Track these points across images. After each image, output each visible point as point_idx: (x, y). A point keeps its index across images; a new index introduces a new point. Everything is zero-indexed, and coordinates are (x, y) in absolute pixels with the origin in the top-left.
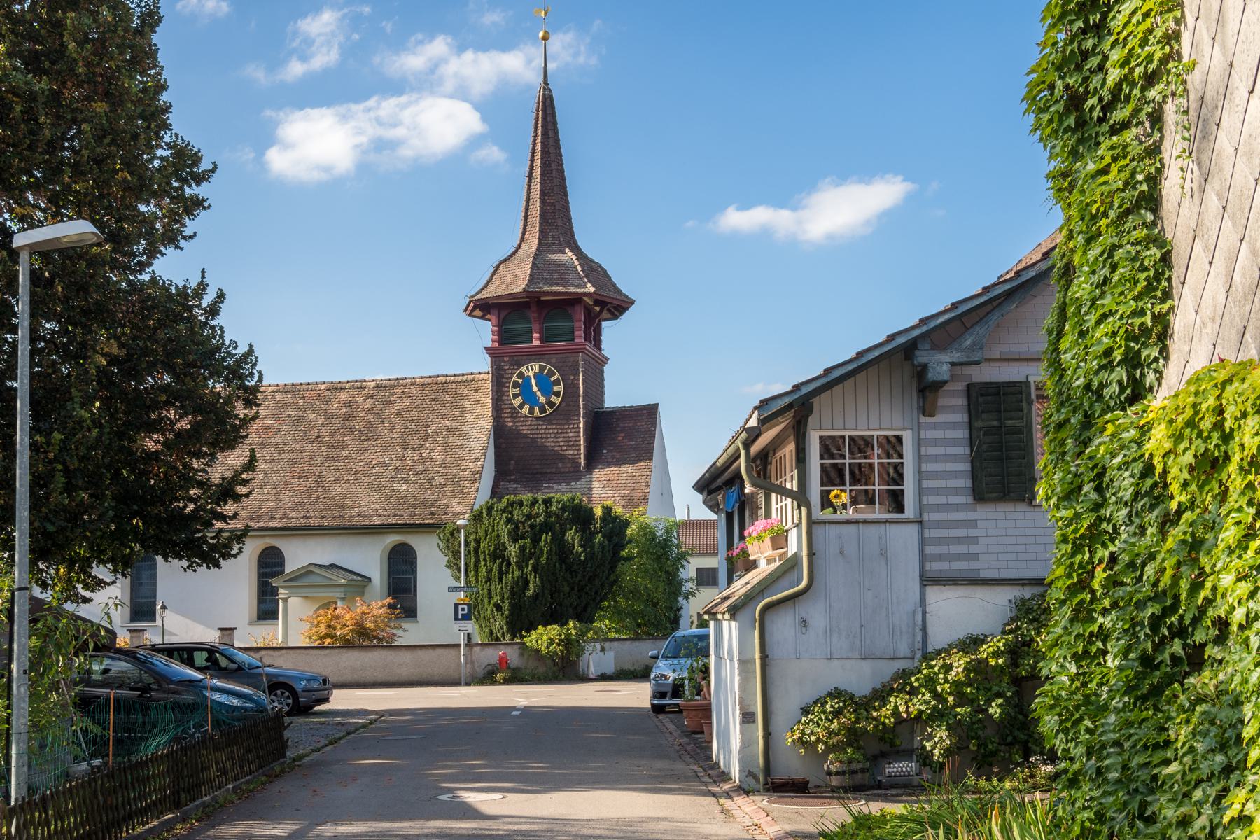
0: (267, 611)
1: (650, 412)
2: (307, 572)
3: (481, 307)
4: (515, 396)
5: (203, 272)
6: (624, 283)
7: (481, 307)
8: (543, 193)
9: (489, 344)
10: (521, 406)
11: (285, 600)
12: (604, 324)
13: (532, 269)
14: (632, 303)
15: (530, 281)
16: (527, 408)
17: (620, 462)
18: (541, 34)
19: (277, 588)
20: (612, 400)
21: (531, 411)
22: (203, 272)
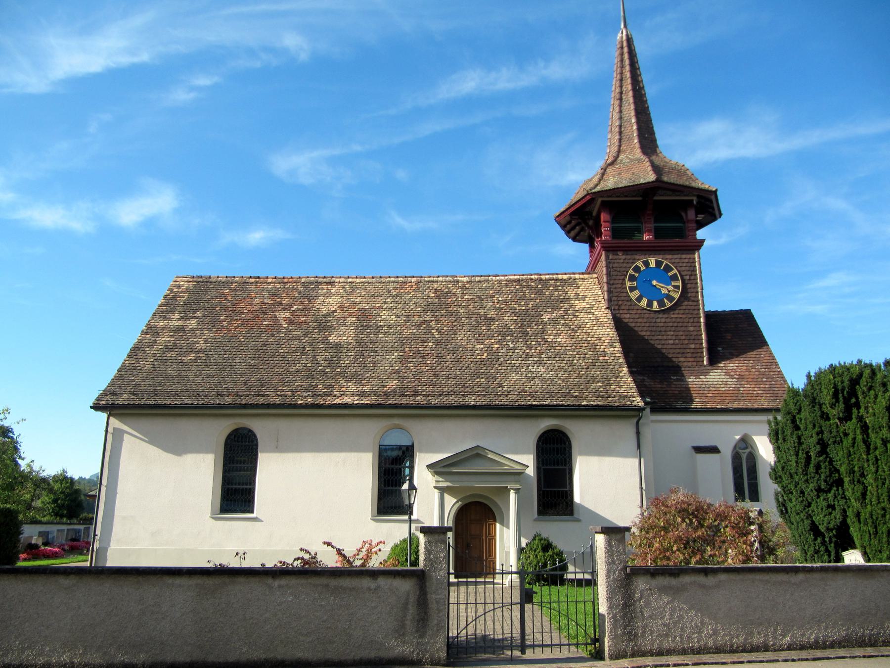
4: (632, 289)
10: (639, 299)
16: (644, 303)
21: (650, 304)
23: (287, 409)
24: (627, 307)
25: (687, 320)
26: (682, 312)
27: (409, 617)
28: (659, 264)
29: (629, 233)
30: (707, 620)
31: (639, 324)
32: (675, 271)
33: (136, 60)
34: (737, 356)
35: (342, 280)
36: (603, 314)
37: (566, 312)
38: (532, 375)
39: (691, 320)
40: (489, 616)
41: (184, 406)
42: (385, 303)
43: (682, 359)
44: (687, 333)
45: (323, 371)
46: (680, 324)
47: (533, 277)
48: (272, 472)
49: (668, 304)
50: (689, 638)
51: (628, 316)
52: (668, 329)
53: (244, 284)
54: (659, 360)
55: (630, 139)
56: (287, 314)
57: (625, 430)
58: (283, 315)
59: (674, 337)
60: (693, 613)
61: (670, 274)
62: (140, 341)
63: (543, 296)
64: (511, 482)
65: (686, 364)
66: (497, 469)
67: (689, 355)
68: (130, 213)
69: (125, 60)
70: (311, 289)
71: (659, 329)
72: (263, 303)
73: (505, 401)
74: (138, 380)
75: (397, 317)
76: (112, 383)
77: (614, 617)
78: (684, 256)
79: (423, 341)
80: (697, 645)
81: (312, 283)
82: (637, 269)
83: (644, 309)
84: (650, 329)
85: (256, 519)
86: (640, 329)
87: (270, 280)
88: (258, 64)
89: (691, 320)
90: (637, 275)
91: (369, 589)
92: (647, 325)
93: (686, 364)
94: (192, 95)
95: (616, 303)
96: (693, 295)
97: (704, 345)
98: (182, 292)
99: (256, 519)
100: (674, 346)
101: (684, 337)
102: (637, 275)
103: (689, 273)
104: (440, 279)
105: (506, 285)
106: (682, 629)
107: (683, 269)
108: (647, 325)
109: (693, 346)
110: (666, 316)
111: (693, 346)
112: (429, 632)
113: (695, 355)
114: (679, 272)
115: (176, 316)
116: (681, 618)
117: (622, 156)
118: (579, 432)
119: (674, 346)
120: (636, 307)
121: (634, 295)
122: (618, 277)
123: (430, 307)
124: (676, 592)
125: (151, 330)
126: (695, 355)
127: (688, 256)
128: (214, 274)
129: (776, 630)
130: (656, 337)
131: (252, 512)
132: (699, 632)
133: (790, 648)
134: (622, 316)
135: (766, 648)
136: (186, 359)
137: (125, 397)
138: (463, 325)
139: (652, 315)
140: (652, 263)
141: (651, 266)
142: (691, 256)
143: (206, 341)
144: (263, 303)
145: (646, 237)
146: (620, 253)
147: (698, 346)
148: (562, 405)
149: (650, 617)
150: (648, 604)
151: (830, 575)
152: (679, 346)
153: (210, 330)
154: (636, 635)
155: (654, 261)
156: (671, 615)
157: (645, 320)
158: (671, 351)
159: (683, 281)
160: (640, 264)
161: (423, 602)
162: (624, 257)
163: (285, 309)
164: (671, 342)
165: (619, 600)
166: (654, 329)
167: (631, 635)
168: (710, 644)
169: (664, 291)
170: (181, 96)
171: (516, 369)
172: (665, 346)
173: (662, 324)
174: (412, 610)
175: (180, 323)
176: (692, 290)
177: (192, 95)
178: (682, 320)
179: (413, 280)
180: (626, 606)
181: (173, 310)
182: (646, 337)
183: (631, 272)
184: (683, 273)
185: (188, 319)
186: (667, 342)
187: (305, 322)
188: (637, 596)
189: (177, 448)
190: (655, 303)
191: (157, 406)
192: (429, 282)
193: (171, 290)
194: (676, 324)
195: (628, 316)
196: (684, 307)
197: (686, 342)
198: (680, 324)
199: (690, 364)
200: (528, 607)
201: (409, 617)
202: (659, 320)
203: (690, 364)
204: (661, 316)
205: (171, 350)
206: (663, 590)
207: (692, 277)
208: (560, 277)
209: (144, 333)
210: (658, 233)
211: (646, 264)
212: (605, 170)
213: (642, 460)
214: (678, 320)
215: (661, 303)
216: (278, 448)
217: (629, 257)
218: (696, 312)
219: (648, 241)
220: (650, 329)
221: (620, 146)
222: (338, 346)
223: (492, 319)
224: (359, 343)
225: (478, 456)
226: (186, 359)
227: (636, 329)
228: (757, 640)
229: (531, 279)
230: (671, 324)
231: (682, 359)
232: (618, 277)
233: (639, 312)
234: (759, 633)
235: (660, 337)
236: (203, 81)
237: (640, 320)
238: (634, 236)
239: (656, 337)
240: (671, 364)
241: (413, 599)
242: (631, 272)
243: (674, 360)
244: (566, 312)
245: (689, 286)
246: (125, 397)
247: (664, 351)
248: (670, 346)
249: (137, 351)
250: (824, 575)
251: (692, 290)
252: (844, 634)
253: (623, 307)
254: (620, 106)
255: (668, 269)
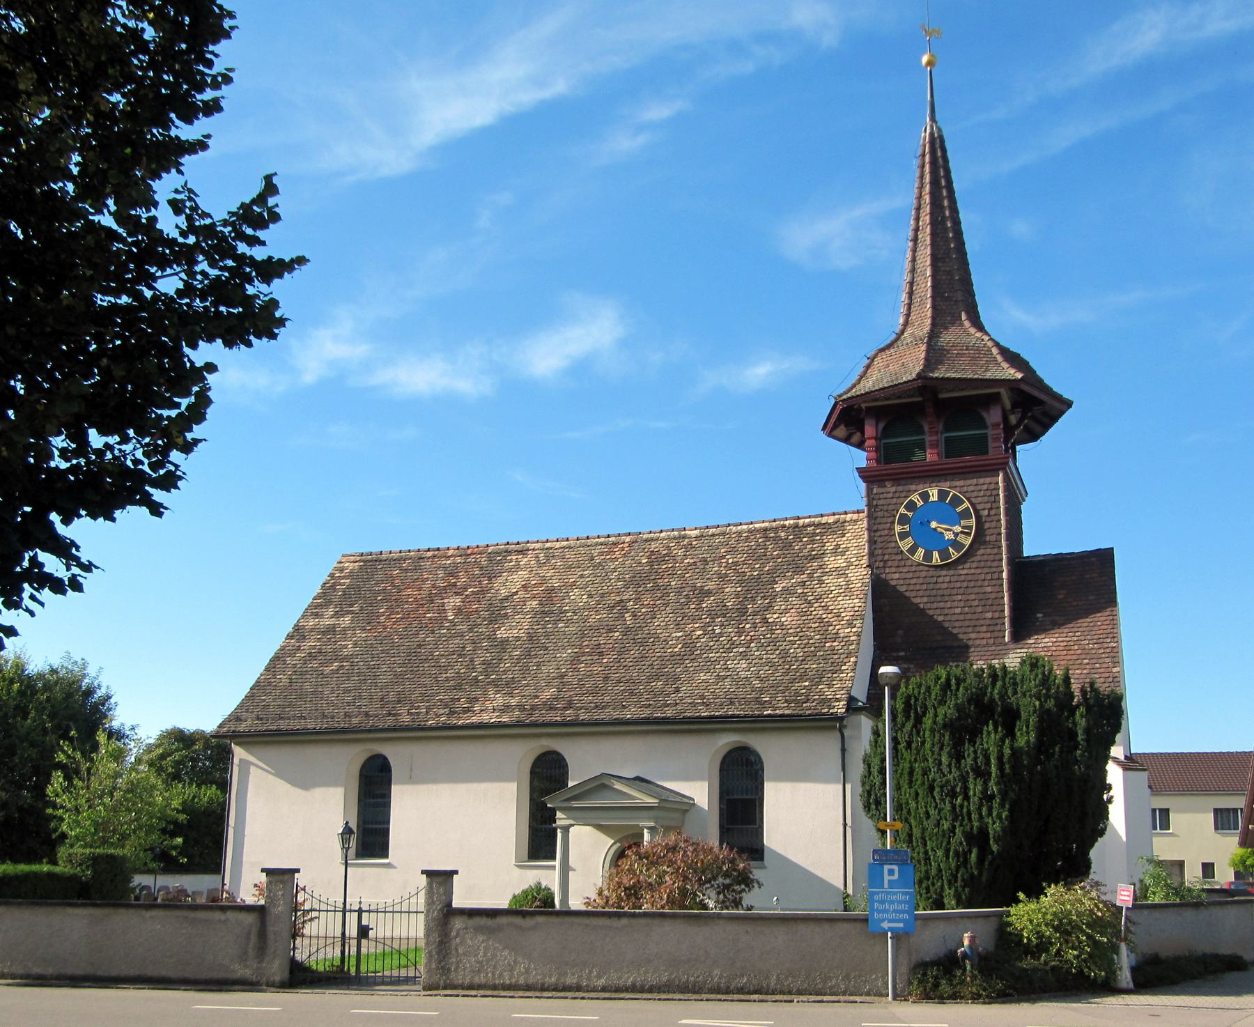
0: (541, 841)
1: (1103, 561)
2: (600, 784)
3: (848, 419)
4: (903, 536)
5: (301, 260)
6: (1054, 375)
7: (848, 419)
8: (934, 257)
9: (864, 464)
10: (913, 550)
11: (566, 829)
12: (1018, 448)
13: (927, 351)
14: (1069, 404)
15: (925, 366)
16: (920, 553)
17: (1055, 625)
18: (925, 59)
19: (553, 811)
20: (1029, 550)
21: (928, 556)
22: (301, 260)
23: (418, 732)
24: (896, 563)
25: (982, 577)
26: (975, 565)
27: (251, 945)
28: (942, 495)
29: (904, 453)
30: (520, 959)
31: (911, 587)
32: (967, 504)
33: (546, 94)
34: (1060, 625)
35: (538, 546)
36: (860, 576)
37: (811, 576)
38: (730, 672)
39: (989, 577)
40: (314, 949)
41: (307, 732)
42: (582, 576)
43: (973, 636)
44: (981, 596)
45: (476, 678)
46: (972, 584)
47: (787, 523)
48: (408, 806)
49: (955, 555)
50: (501, 975)
51: (897, 576)
52: (954, 591)
53: (420, 558)
54: (939, 638)
55: (922, 303)
56: (457, 601)
57: (827, 745)
58: (454, 602)
59: (962, 604)
60: (506, 952)
61: (958, 510)
62: (283, 648)
63: (791, 547)
64: (644, 819)
65: (978, 642)
66: (627, 803)
67: (984, 629)
68: (547, 356)
69: (528, 98)
70: (495, 560)
71: (941, 592)
72: (434, 586)
73: (669, 712)
74: (269, 699)
75: (590, 596)
76: (240, 706)
77: (430, 952)
78: (981, 481)
79: (610, 631)
80: (508, 982)
81: (499, 553)
82: (911, 506)
83: (919, 564)
84: (928, 593)
85: (389, 865)
86: (914, 594)
87: (450, 553)
88: (748, 67)
89: (989, 577)
90: (910, 514)
91: (220, 921)
92: (924, 587)
93: (978, 642)
94: (642, 139)
95: (880, 558)
96: (993, 538)
97: (1007, 612)
98: (344, 577)
99: (389, 865)
100: (962, 617)
101: (976, 603)
102: (910, 514)
103: (989, 505)
104: (663, 535)
105: (747, 538)
106: (495, 967)
107: (979, 500)
108: (924, 587)
109: (989, 615)
110: (952, 572)
111: (989, 615)
112: (267, 959)
113: (991, 628)
114: (972, 504)
115: (331, 611)
116: (494, 956)
117: (909, 331)
118: (768, 747)
119: (962, 617)
120: (909, 563)
121: (905, 545)
122: (885, 520)
123: (636, 581)
124: (491, 931)
125: (298, 633)
126: (991, 628)
127: (988, 480)
128: (385, 549)
129: (591, 972)
130: (935, 605)
131: (387, 856)
132: (512, 970)
133: (604, 989)
134: (889, 577)
135: (578, 988)
136: (327, 670)
137: (249, 722)
138: (667, 605)
139: (931, 573)
140: (934, 494)
141: (932, 499)
142: (993, 480)
143: (355, 644)
144: (434, 586)
145: (930, 456)
146: (888, 484)
147: (997, 615)
148: (738, 716)
149: (464, 954)
150: (462, 943)
151: (657, 921)
152: (969, 616)
153: (363, 629)
154: (449, 970)
155: (935, 492)
156: (485, 954)
157: (921, 581)
158: (957, 624)
159: (978, 518)
160: (915, 497)
161: (262, 934)
162: (894, 489)
163: (457, 594)
164: (958, 611)
165: (436, 937)
166: (934, 592)
167: (445, 970)
168: (522, 981)
169: (949, 536)
170: (623, 144)
171: (708, 666)
172: (949, 618)
173: (945, 585)
174: (253, 939)
175: (332, 621)
176: (992, 531)
177: (642, 139)
178: (975, 577)
179: (628, 539)
180: (441, 943)
181: (326, 605)
182: (922, 606)
183: (902, 510)
184: (979, 507)
185: (343, 616)
186: (952, 611)
187: (476, 610)
188: (454, 934)
189: (304, 783)
190: (936, 555)
191: (278, 733)
192: (646, 540)
193: (332, 575)
194: (965, 584)
195: (897, 576)
196: (979, 558)
197: (980, 609)
198: (972, 584)
199: (984, 642)
200: (364, 942)
201: (251, 945)
202: (940, 580)
203: (984, 642)
204: (944, 572)
205: (315, 658)
206: (479, 930)
207: (993, 512)
208: (824, 520)
209: (290, 637)
210: (952, 449)
211: (925, 496)
212: (873, 360)
213: (848, 787)
214: (970, 577)
215: (944, 554)
216: (412, 779)
217: (900, 488)
218: (995, 564)
219: (932, 464)
220: (928, 593)
221: (908, 315)
222: (504, 642)
223: (709, 593)
224: (531, 637)
225: (604, 787)
226: (327, 670)
227: (908, 594)
228: (570, 980)
229: (784, 526)
230: (958, 585)
231: (973, 636)
232: (885, 520)
233: (914, 569)
234: (573, 974)
235: (942, 605)
236: (658, 112)
237: (914, 581)
238: (913, 454)
239: (935, 605)
240: (956, 644)
241: (254, 930)
242: (902, 510)
243: (961, 636)
244: (811, 576)
245: (987, 526)
246: (249, 722)
247: (946, 625)
248: (955, 617)
249: (277, 660)
250: (649, 920)
251: (992, 531)
252: (665, 979)
253: (890, 563)
254: (914, 251)
255: (956, 501)
